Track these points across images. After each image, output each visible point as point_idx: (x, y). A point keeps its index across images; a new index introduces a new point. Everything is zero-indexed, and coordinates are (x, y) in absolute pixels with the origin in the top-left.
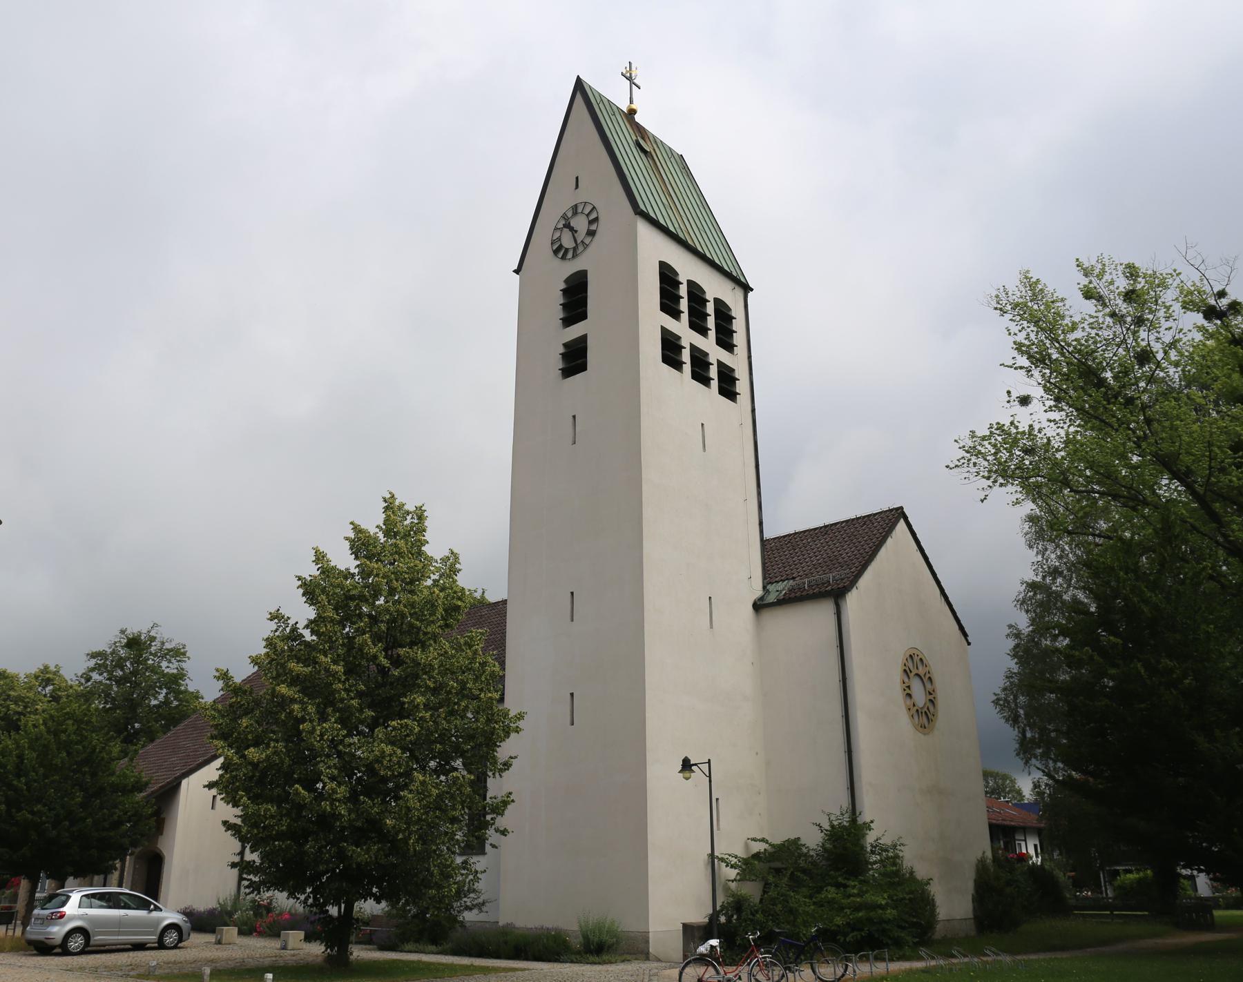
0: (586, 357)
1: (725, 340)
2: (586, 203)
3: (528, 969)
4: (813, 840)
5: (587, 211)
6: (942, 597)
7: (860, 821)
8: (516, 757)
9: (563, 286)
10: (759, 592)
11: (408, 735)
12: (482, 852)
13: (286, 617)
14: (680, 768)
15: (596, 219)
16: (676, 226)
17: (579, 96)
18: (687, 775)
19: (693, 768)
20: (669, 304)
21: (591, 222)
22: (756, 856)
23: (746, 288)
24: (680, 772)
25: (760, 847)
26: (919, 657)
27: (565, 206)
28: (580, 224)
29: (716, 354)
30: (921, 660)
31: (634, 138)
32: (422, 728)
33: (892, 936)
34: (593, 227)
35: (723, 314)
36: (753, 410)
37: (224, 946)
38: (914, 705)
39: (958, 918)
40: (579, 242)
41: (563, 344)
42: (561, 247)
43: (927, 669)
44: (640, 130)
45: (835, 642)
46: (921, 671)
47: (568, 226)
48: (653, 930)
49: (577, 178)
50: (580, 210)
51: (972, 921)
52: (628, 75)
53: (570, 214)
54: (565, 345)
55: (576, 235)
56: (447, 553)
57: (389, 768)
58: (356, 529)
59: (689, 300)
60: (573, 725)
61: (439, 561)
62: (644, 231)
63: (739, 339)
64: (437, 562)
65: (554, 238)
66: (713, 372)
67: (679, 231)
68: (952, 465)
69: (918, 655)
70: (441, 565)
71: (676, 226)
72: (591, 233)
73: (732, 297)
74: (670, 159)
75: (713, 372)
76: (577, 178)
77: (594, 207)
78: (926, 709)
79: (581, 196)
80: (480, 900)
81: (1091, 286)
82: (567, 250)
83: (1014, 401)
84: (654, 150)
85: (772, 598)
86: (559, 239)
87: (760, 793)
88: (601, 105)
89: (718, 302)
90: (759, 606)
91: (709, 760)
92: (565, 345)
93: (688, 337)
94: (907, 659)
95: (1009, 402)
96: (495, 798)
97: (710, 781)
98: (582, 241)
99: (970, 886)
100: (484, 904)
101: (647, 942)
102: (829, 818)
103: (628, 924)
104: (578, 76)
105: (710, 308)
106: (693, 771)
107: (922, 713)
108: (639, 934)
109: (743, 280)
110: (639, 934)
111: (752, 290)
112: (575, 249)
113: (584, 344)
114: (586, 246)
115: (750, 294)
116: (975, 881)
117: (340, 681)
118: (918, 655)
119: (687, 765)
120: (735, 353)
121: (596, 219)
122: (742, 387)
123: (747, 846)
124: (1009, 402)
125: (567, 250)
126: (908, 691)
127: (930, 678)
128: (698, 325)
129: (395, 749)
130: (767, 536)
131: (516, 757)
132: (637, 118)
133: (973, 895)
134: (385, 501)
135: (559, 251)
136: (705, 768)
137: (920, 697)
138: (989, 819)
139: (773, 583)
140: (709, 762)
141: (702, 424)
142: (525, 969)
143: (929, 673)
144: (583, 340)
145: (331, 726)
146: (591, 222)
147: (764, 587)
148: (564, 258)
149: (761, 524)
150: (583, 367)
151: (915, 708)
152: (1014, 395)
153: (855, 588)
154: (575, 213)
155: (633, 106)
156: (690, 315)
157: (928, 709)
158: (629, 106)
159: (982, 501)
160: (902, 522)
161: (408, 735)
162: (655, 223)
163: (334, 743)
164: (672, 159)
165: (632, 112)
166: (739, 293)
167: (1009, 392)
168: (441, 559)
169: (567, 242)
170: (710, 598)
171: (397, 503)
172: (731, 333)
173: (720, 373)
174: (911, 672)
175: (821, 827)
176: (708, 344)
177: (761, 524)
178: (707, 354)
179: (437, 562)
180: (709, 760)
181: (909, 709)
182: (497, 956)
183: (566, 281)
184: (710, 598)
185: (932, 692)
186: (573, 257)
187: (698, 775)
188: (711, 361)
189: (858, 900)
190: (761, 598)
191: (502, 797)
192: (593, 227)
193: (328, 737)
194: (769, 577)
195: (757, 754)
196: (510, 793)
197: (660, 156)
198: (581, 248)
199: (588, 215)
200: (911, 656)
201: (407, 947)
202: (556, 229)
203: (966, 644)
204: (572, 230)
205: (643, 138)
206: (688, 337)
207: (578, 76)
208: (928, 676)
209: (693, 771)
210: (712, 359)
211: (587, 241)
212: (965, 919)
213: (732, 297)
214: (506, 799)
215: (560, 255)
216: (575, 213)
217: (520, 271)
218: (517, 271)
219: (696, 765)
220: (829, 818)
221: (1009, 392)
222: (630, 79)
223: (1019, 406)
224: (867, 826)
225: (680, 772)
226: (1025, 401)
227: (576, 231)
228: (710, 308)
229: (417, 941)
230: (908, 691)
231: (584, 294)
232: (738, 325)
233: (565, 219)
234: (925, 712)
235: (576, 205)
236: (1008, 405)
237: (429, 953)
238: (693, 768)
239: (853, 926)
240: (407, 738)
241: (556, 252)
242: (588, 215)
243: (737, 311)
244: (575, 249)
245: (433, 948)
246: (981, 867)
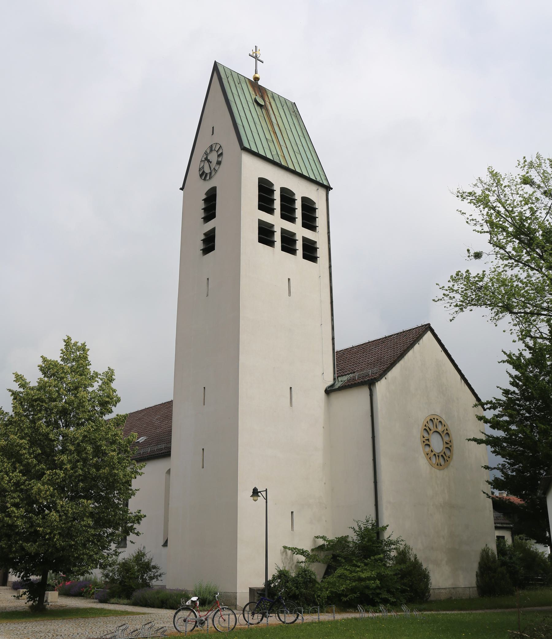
0: (214, 242)
2: (217, 143)
3: (148, 614)
4: (353, 537)
5: (217, 149)
6: (462, 380)
7: (380, 526)
8: (138, 490)
9: (204, 197)
10: (331, 382)
11: (57, 479)
12: (125, 546)
13: (5, 412)
15: (222, 154)
16: (274, 153)
18: (255, 498)
19: (259, 494)
22: (321, 548)
23: (328, 188)
24: (251, 496)
25: (321, 542)
26: (438, 420)
27: (206, 147)
28: (213, 157)
30: (440, 422)
31: (254, 96)
32: (66, 474)
33: (381, 597)
36: (330, 267)
37: (20, 600)
38: (432, 451)
39: (463, 586)
40: (212, 169)
41: (204, 234)
42: (204, 172)
43: (445, 428)
44: (261, 91)
45: (370, 414)
46: (440, 428)
47: (206, 159)
48: (240, 592)
49: (213, 127)
51: (476, 589)
52: (255, 54)
53: (208, 151)
54: (205, 234)
55: (211, 165)
56: (107, 370)
57: (45, 499)
58: (45, 360)
60: (203, 468)
61: (102, 375)
63: (321, 222)
64: (100, 375)
65: (200, 167)
68: (436, 299)
69: (437, 419)
70: (103, 377)
72: (219, 163)
76: (213, 127)
77: (221, 146)
78: (442, 454)
79: (216, 139)
80: (158, 573)
81: (528, 175)
82: (207, 174)
83: (472, 256)
85: (338, 385)
86: (203, 167)
87: (326, 508)
88: (230, 79)
89: (284, 191)
90: (329, 391)
91: (266, 489)
92: (205, 234)
94: (427, 422)
95: (469, 257)
96: (132, 514)
97: (266, 502)
98: (214, 169)
99: (475, 567)
100: (160, 576)
101: (236, 599)
102: (358, 524)
103: (223, 588)
106: (259, 496)
107: (438, 456)
108: (232, 594)
110: (232, 594)
111: (332, 189)
112: (210, 173)
113: (213, 234)
115: (331, 192)
116: (479, 563)
117: (25, 449)
118: (437, 419)
120: (317, 231)
121: (222, 154)
122: (322, 253)
123: (315, 542)
124: (469, 257)
125: (207, 174)
126: (427, 442)
127: (448, 434)
129: (50, 487)
130: (429, 333)
131: (138, 490)
133: (477, 572)
134: (65, 341)
135: (203, 175)
136: (264, 493)
137: (437, 444)
138: (495, 523)
139: (343, 376)
141: (289, 279)
142: (144, 614)
143: (447, 430)
144: (213, 231)
145: (17, 475)
147: (334, 379)
149: (333, 339)
151: (433, 453)
152: (472, 253)
153: (384, 378)
154: (211, 150)
155: (257, 76)
157: (444, 453)
158: (254, 75)
159: (451, 321)
160: (429, 333)
161: (57, 479)
163: (17, 484)
166: (322, 192)
167: (468, 250)
168: (103, 374)
170: (291, 388)
171: (73, 342)
174: (430, 430)
175: (354, 529)
177: (333, 339)
178: (294, 234)
179: (100, 375)
180: (266, 489)
181: (427, 454)
182: (153, 607)
184: (291, 388)
185: (449, 443)
187: (261, 500)
190: (332, 386)
191: (135, 513)
192: (220, 159)
193: (14, 481)
194: (339, 371)
195: (325, 483)
196: (140, 511)
198: (213, 173)
200: (431, 420)
201: (112, 600)
202: (202, 161)
203: (483, 410)
204: (209, 161)
208: (445, 432)
209: (259, 496)
212: (469, 587)
214: (137, 514)
216: (211, 150)
217: (183, 189)
218: (182, 189)
219: (260, 492)
220: (358, 524)
221: (468, 250)
222: (256, 58)
223: (474, 259)
224: (385, 528)
225: (251, 496)
226: (478, 255)
227: (211, 162)
229: (120, 597)
230: (427, 442)
231: (214, 202)
232: (320, 214)
233: (206, 154)
234: (442, 456)
235: (212, 145)
236: (468, 259)
237: (122, 604)
239: (353, 590)
240: (57, 481)
241: (201, 176)
244: (210, 173)
245: (126, 601)
246: (485, 556)
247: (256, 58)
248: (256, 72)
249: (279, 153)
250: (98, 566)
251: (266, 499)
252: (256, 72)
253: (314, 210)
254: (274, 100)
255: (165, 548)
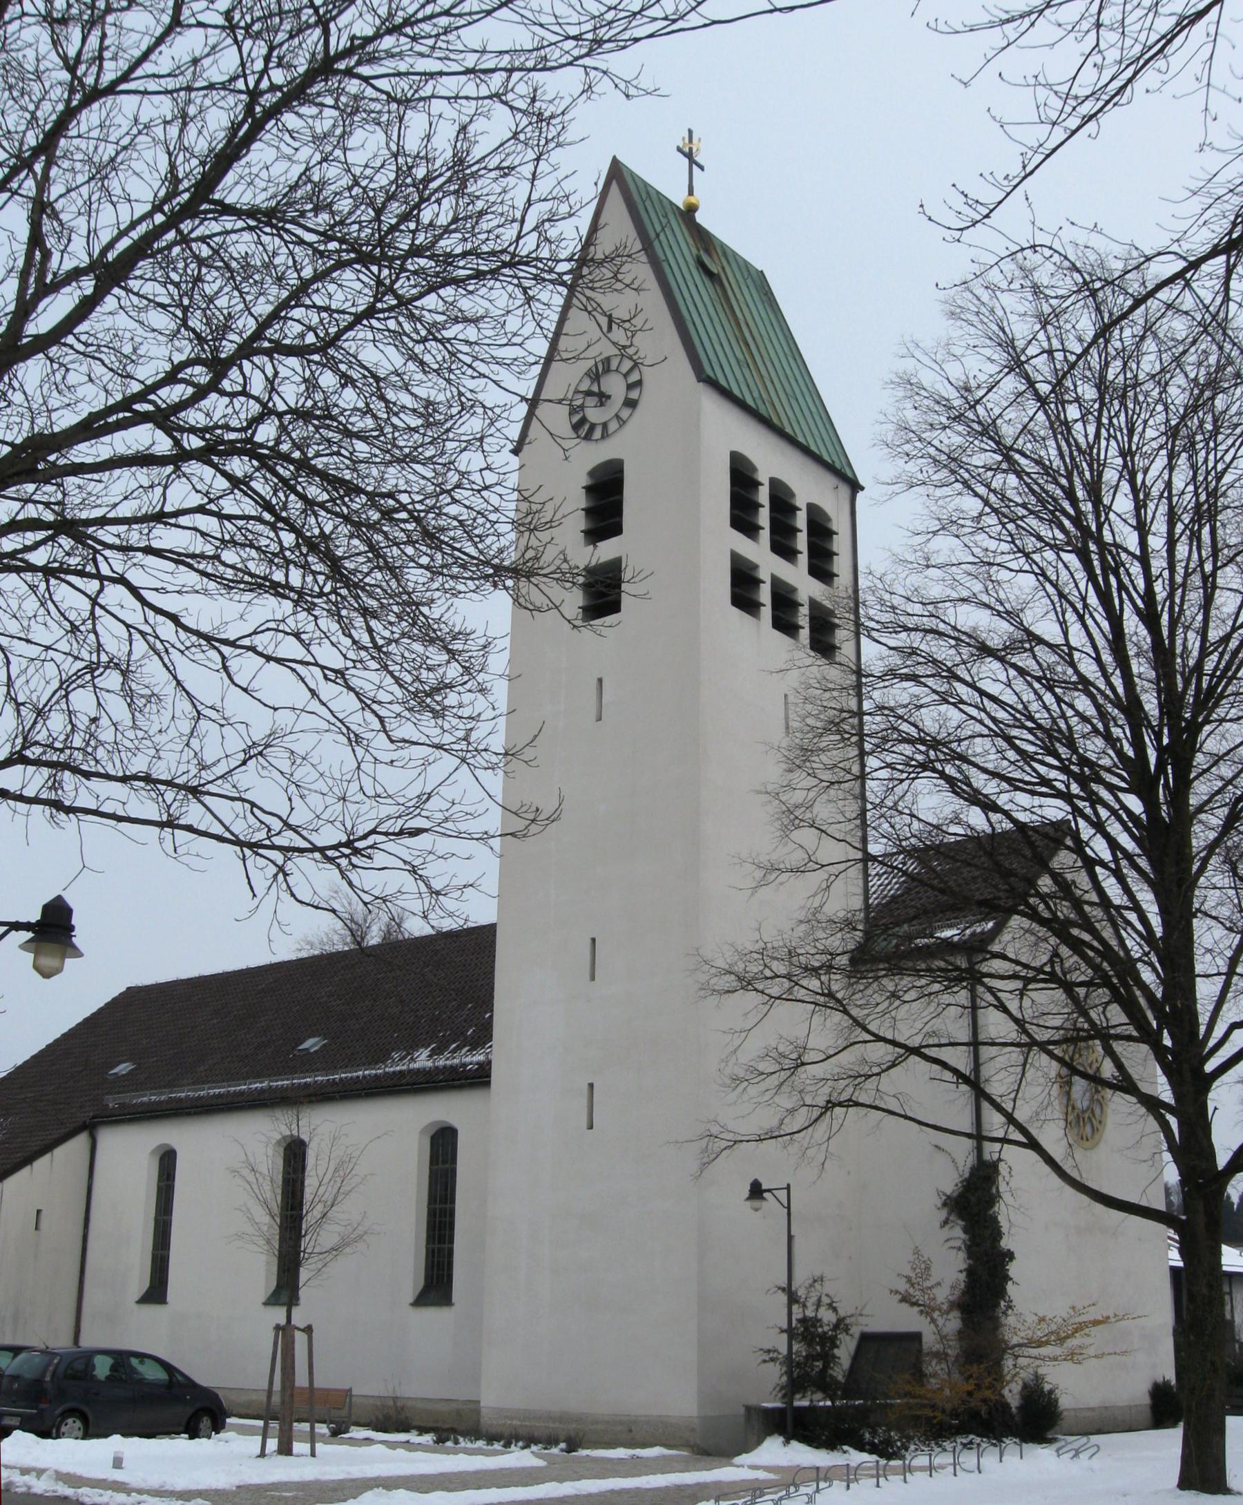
1: (821, 569)
14: (746, 1194)
15: (639, 383)
16: (756, 394)
17: (615, 189)
19: (766, 1195)
20: (743, 520)
21: (630, 387)
23: (855, 487)
24: (748, 1199)
28: (615, 386)
29: (807, 588)
31: (695, 251)
34: (634, 395)
35: (820, 530)
42: (583, 420)
44: (703, 238)
50: (613, 367)
59: (772, 510)
62: (712, 407)
63: (841, 565)
66: (765, 595)
67: (759, 402)
71: (756, 394)
72: (631, 404)
73: (830, 499)
74: (644, 202)
75: (765, 595)
82: (593, 427)
84: (723, 268)
88: (648, 203)
89: (775, 484)
93: (768, 565)
97: (789, 1214)
104: (614, 157)
105: (763, 495)
106: (764, 1199)
109: (849, 474)
111: (862, 488)
114: (622, 422)
115: (860, 495)
119: (757, 1191)
121: (639, 383)
125: (593, 427)
128: (784, 549)
132: (700, 217)
135: (583, 428)
136: (782, 1195)
140: (788, 1188)
146: (630, 387)
148: (588, 437)
150: (614, 607)
155: (692, 200)
156: (773, 532)
162: (726, 394)
164: (749, 281)
165: (692, 209)
166: (844, 491)
169: (594, 414)
172: (830, 555)
173: (813, 619)
176: (798, 576)
178: (756, 567)
183: (591, 474)
186: (603, 437)
188: (800, 601)
189: (320, 1078)
192: (634, 395)
197: (731, 276)
199: (626, 376)
205: (707, 251)
206: (768, 565)
207: (614, 157)
209: (764, 1199)
210: (764, 574)
211: (625, 413)
213: (830, 499)
215: (583, 432)
219: (769, 1191)
222: (689, 156)
225: (748, 1199)
228: (763, 495)
232: (840, 544)
238: (766, 1195)
241: (576, 427)
242: (626, 376)
243: (839, 523)
247: (689, 156)
248: (691, 193)
249: (764, 396)
250: (845, 1351)
251: (789, 1208)
252: (691, 193)
253: (829, 534)
254: (728, 262)
255: (433, 1315)
